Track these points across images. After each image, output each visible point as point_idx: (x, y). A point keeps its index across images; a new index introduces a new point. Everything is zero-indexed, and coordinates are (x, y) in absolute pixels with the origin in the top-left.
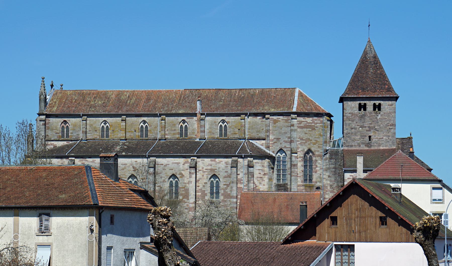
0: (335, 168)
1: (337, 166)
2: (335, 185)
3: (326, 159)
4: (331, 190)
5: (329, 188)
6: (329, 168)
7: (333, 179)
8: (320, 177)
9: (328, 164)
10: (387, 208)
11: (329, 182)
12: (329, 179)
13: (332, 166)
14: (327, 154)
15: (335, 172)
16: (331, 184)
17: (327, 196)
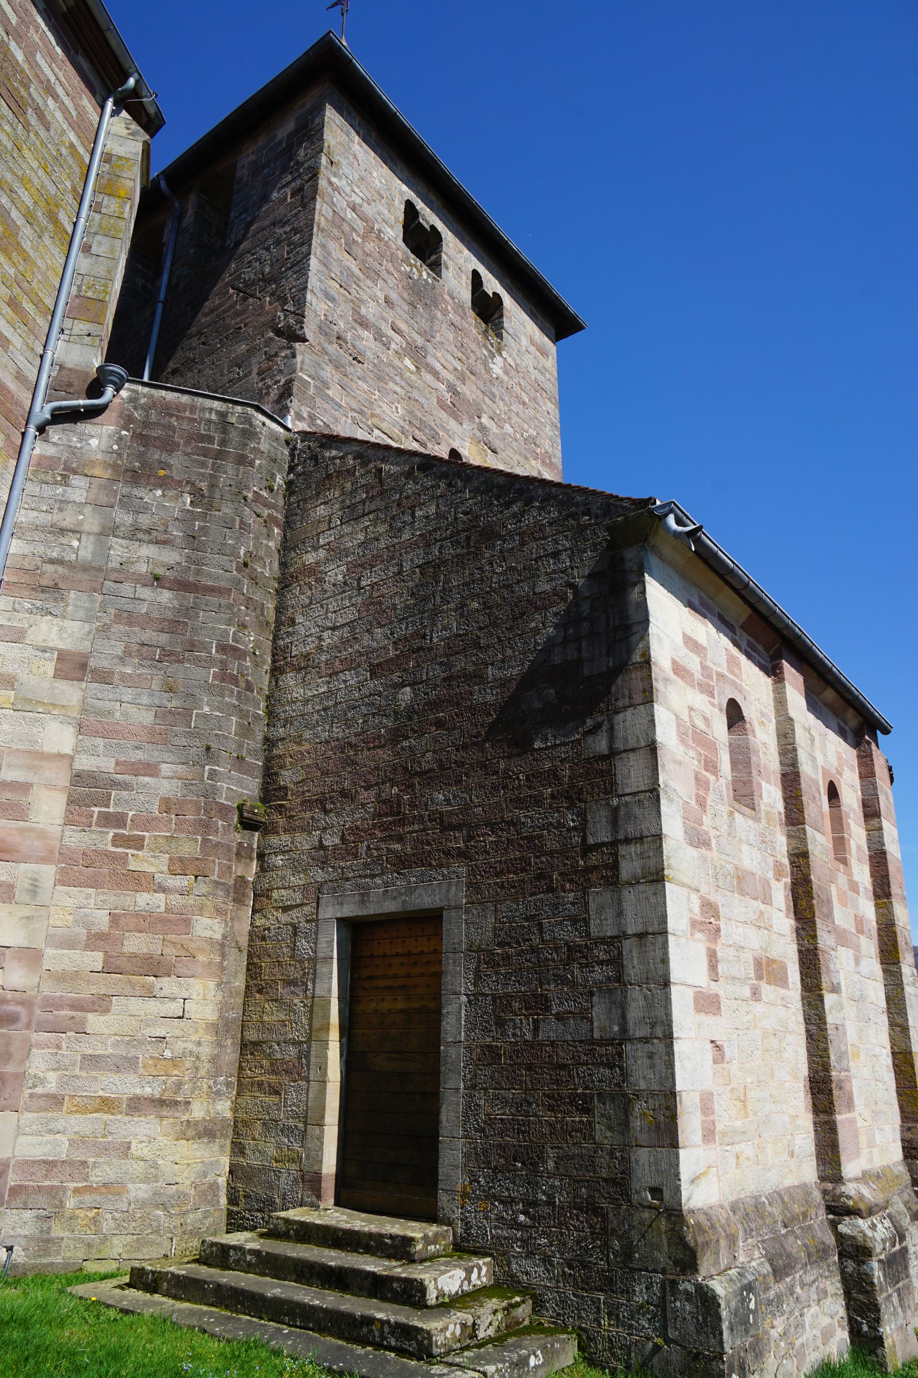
0: (181, 586)
1: (216, 569)
2: (166, 783)
3: (67, 469)
4: (75, 839)
5: (49, 808)
6: (96, 575)
7: (134, 708)
8: (279, 297)
9: (91, 522)
10: (264, 1254)
11: (60, 737)
12: (72, 693)
13: (147, 556)
14: (93, 413)
15: (172, 626)
16: (99, 760)
17: (546, 445)
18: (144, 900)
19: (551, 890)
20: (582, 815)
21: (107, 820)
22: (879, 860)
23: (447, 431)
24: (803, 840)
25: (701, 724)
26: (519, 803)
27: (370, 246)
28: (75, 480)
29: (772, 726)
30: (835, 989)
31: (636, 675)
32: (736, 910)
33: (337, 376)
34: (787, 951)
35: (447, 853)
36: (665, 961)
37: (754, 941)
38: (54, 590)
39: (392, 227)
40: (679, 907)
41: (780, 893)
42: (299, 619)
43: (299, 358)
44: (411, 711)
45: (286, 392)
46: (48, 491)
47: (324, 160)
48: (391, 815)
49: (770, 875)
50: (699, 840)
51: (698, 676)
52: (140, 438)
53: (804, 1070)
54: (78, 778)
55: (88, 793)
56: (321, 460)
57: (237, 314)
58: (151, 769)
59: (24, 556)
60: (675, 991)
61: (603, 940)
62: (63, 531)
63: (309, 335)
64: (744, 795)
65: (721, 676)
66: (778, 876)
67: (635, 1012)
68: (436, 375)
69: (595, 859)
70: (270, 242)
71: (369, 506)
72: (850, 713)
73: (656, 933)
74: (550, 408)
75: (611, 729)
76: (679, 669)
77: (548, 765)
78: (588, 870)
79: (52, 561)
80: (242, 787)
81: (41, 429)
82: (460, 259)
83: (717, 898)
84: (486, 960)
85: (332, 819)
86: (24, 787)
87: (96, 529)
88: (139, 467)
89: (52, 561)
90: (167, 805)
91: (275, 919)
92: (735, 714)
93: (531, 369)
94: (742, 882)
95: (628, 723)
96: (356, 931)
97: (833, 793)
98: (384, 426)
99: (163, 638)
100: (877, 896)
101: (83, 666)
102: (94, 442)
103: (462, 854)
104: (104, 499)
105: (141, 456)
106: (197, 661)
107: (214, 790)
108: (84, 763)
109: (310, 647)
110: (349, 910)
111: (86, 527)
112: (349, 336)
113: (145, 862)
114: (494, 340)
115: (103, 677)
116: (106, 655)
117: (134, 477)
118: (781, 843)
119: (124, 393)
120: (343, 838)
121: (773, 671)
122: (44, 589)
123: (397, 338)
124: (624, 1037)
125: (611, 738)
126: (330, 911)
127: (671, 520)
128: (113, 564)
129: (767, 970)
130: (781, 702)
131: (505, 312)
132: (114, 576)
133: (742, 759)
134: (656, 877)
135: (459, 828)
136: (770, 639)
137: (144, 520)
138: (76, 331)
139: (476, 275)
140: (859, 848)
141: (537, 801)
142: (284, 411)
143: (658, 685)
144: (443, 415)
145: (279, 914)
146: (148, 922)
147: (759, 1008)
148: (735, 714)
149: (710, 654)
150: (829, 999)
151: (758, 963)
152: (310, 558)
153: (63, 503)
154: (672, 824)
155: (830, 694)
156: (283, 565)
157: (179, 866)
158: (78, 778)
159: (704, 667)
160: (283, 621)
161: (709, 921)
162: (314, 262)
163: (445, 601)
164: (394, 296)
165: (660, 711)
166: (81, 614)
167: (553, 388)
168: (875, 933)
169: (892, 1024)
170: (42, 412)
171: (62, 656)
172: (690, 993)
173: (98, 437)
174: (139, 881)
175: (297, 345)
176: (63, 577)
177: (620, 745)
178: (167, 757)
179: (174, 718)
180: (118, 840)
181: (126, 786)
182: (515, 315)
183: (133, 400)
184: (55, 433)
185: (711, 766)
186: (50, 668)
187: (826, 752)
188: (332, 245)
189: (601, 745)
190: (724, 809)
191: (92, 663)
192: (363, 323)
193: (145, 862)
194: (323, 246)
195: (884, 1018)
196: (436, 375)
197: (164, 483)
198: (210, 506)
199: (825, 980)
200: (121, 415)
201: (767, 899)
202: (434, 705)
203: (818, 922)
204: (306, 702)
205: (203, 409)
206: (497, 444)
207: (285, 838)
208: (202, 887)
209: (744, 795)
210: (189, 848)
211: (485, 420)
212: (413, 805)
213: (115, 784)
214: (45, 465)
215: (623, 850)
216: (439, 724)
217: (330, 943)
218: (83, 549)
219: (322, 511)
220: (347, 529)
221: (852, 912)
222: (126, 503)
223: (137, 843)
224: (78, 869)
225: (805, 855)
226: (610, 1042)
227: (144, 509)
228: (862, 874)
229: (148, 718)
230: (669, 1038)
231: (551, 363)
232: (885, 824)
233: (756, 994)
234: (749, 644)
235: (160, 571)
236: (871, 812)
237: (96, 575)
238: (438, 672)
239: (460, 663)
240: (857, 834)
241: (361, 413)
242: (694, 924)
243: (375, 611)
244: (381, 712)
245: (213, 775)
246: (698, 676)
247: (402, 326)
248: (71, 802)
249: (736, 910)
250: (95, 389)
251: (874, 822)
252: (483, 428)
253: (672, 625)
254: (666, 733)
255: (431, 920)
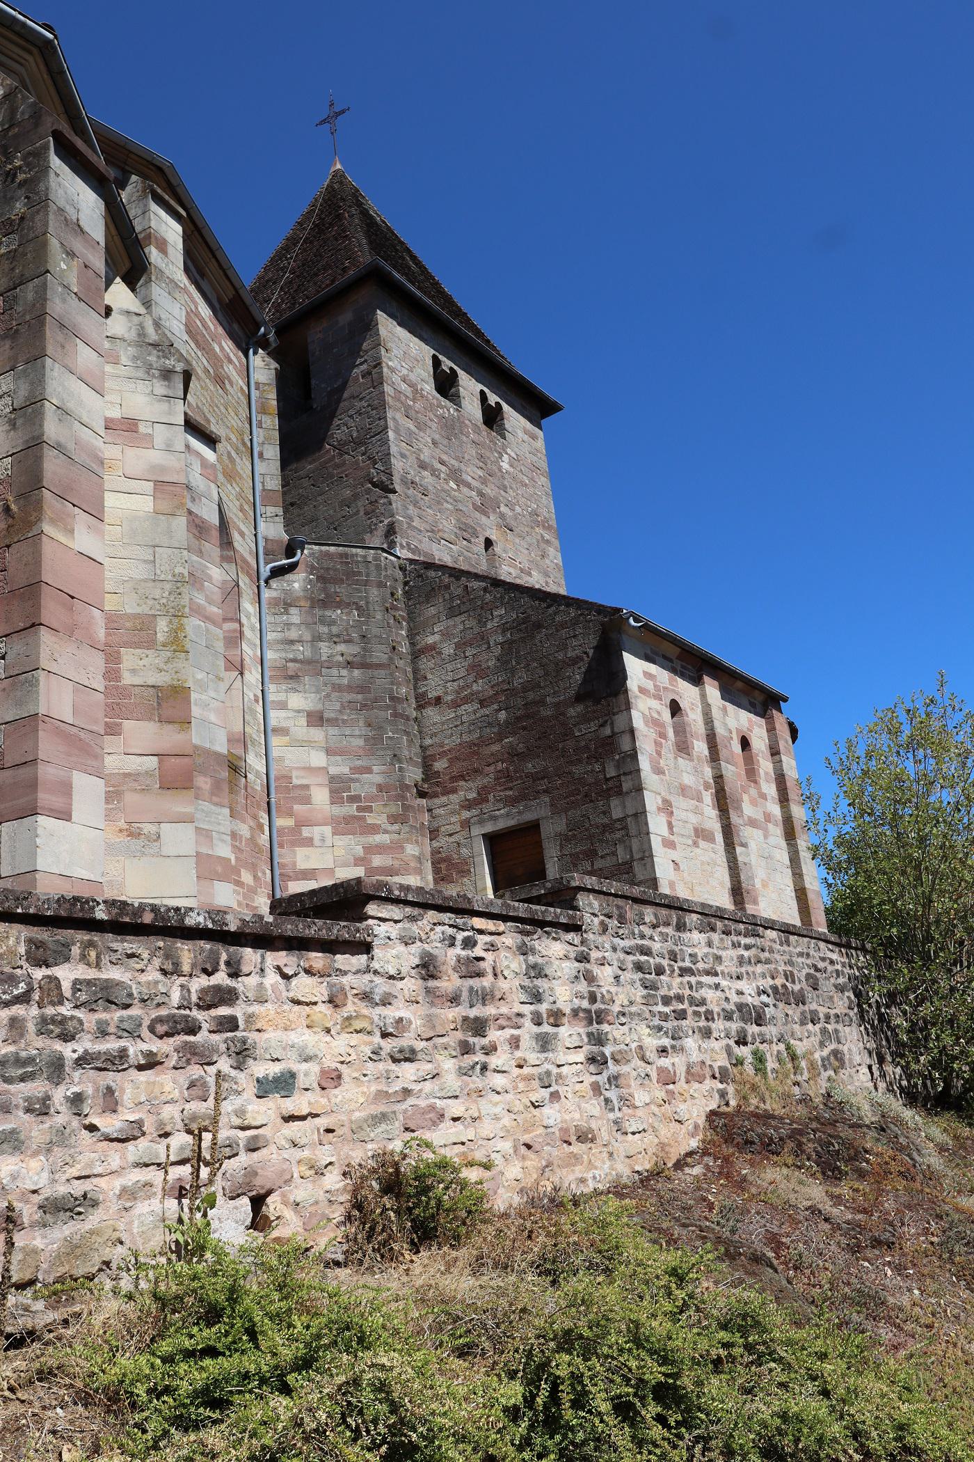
1: (379, 654)
4: (339, 811)
5: (321, 796)
11: (318, 759)
12: (318, 734)
14: (291, 568)
16: (341, 768)
18: (379, 838)
19: (591, 801)
20: (603, 765)
21: (353, 799)
22: (781, 780)
23: (480, 526)
24: (720, 769)
25: (656, 716)
26: (571, 763)
27: (418, 406)
28: (293, 610)
29: (699, 710)
30: (744, 845)
31: (622, 697)
32: (682, 806)
33: (416, 511)
34: (716, 827)
35: (538, 792)
36: (647, 824)
37: (694, 819)
38: (294, 677)
39: (427, 383)
40: (651, 802)
41: (708, 797)
42: (430, 676)
43: (394, 505)
44: (506, 722)
45: (391, 531)
46: (279, 619)
47: (383, 351)
48: (505, 778)
49: (702, 788)
50: (658, 771)
51: (652, 691)
52: (321, 578)
53: (728, 885)
54: (333, 779)
55: (338, 788)
56: (426, 581)
57: (337, 466)
58: (368, 770)
59: (275, 660)
60: (652, 837)
61: (618, 820)
62: (292, 642)
63: (398, 488)
64: (683, 747)
65: (665, 688)
66: (707, 787)
67: (635, 848)
68: (469, 486)
69: (610, 784)
70: (351, 412)
71: (463, 608)
72: (757, 693)
73: (640, 814)
74: (543, 481)
75: (612, 724)
76: (642, 690)
77: (583, 743)
78: (609, 789)
79: (292, 660)
80: (414, 774)
81: (266, 582)
82: (469, 386)
83: (671, 798)
84: (564, 839)
85: (470, 784)
86: (307, 787)
87: (309, 638)
88: (324, 598)
89: (292, 660)
90: (380, 788)
91: (442, 842)
92: (675, 708)
93: (527, 455)
94: (683, 790)
95: (619, 721)
96: (493, 841)
97: (745, 743)
98: (445, 536)
99: (360, 697)
100: (781, 802)
101: (321, 718)
102: (296, 585)
103: (546, 791)
104: (310, 620)
105: (325, 589)
106: (380, 708)
107: (403, 777)
108: (333, 770)
109: (439, 693)
110: (489, 828)
111: (304, 638)
112: (417, 479)
113: (371, 819)
114: (500, 441)
115: (333, 722)
116: (331, 711)
117: (326, 603)
118: (708, 773)
119: (306, 552)
120: (479, 793)
121: (697, 681)
122: (291, 677)
123: (443, 468)
124: (632, 859)
125: (612, 728)
126: (477, 831)
127: (631, 621)
128: (324, 658)
129: (701, 834)
130: (703, 696)
131: (505, 416)
132: (326, 664)
133: (681, 730)
134: (639, 789)
135: (543, 778)
136: (693, 664)
137: (335, 630)
138: (268, 514)
139: (482, 392)
140: (766, 773)
141: (580, 761)
142: (392, 544)
143: (632, 700)
144: (477, 515)
145: (447, 838)
146: (380, 849)
147: (698, 851)
148: (675, 708)
149: (658, 678)
150: (739, 850)
151: (696, 830)
152: (431, 640)
153: (288, 625)
154: (644, 764)
155: (739, 684)
156: (412, 644)
157: (393, 819)
158: (333, 779)
159: (655, 686)
160: (418, 677)
161: (667, 808)
162: (391, 434)
163: (518, 663)
164: (437, 437)
165: (634, 713)
166: (313, 689)
167: (544, 465)
168: (781, 823)
169: (794, 874)
170: (265, 571)
171: (310, 715)
172: (660, 839)
173: (297, 582)
174: (375, 829)
175: (391, 496)
176: (299, 669)
177: (616, 730)
178: (374, 762)
179: (374, 742)
180: (359, 809)
181: (357, 780)
182: (513, 419)
183: (312, 555)
184: (274, 583)
185: (663, 735)
186: (303, 721)
187: (736, 720)
188: (398, 416)
189: (607, 731)
190: (671, 756)
191: (326, 715)
192: (423, 466)
193: (371, 819)
194: (394, 419)
195: (789, 871)
196: (469, 486)
197: (339, 605)
198: (369, 616)
199: (736, 840)
200: (307, 566)
201: (700, 799)
202: (518, 719)
203: (731, 811)
204: (443, 724)
205: (353, 555)
206: (513, 523)
207: (444, 799)
208: (406, 828)
209: (683, 747)
210: (395, 808)
211: (503, 509)
212: (516, 772)
213: (353, 780)
214: (275, 602)
215: (623, 778)
216: (524, 728)
217: (481, 848)
218: (302, 651)
219: (433, 611)
220: (451, 622)
221: (761, 811)
222: (322, 621)
223: (369, 809)
224: (344, 826)
225: (721, 776)
226: (626, 863)
227: (332, 623)
228: (771, 789)
229: (361, 742)
230: (651, 856)
231: (540, 444)
232: (784, 758)
233: (695, 844)
234: (682, 667)
235: (350, 659)
236: (775, 752)
237: (314, 665)
238: (520, 702)
239: (531, 696)
240: (765, 766)
241: (432, 531)
242: (659, 809)
243: (477, 670)
244: (490, 725)
245: (401, 769)
246: (652, 691)
247: (445, 457)
248: (331, 791)
249: (682, 806)
250: (290, 551)
251: (777, 757)
252: (502, 516)
253: (636, 668)
254: (638, 722)
255: (533, 828)
